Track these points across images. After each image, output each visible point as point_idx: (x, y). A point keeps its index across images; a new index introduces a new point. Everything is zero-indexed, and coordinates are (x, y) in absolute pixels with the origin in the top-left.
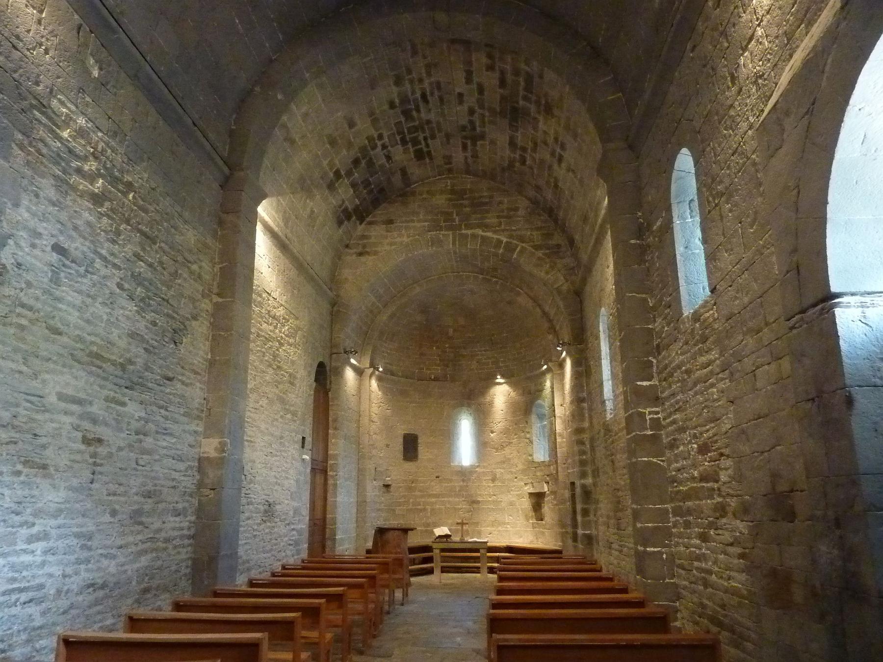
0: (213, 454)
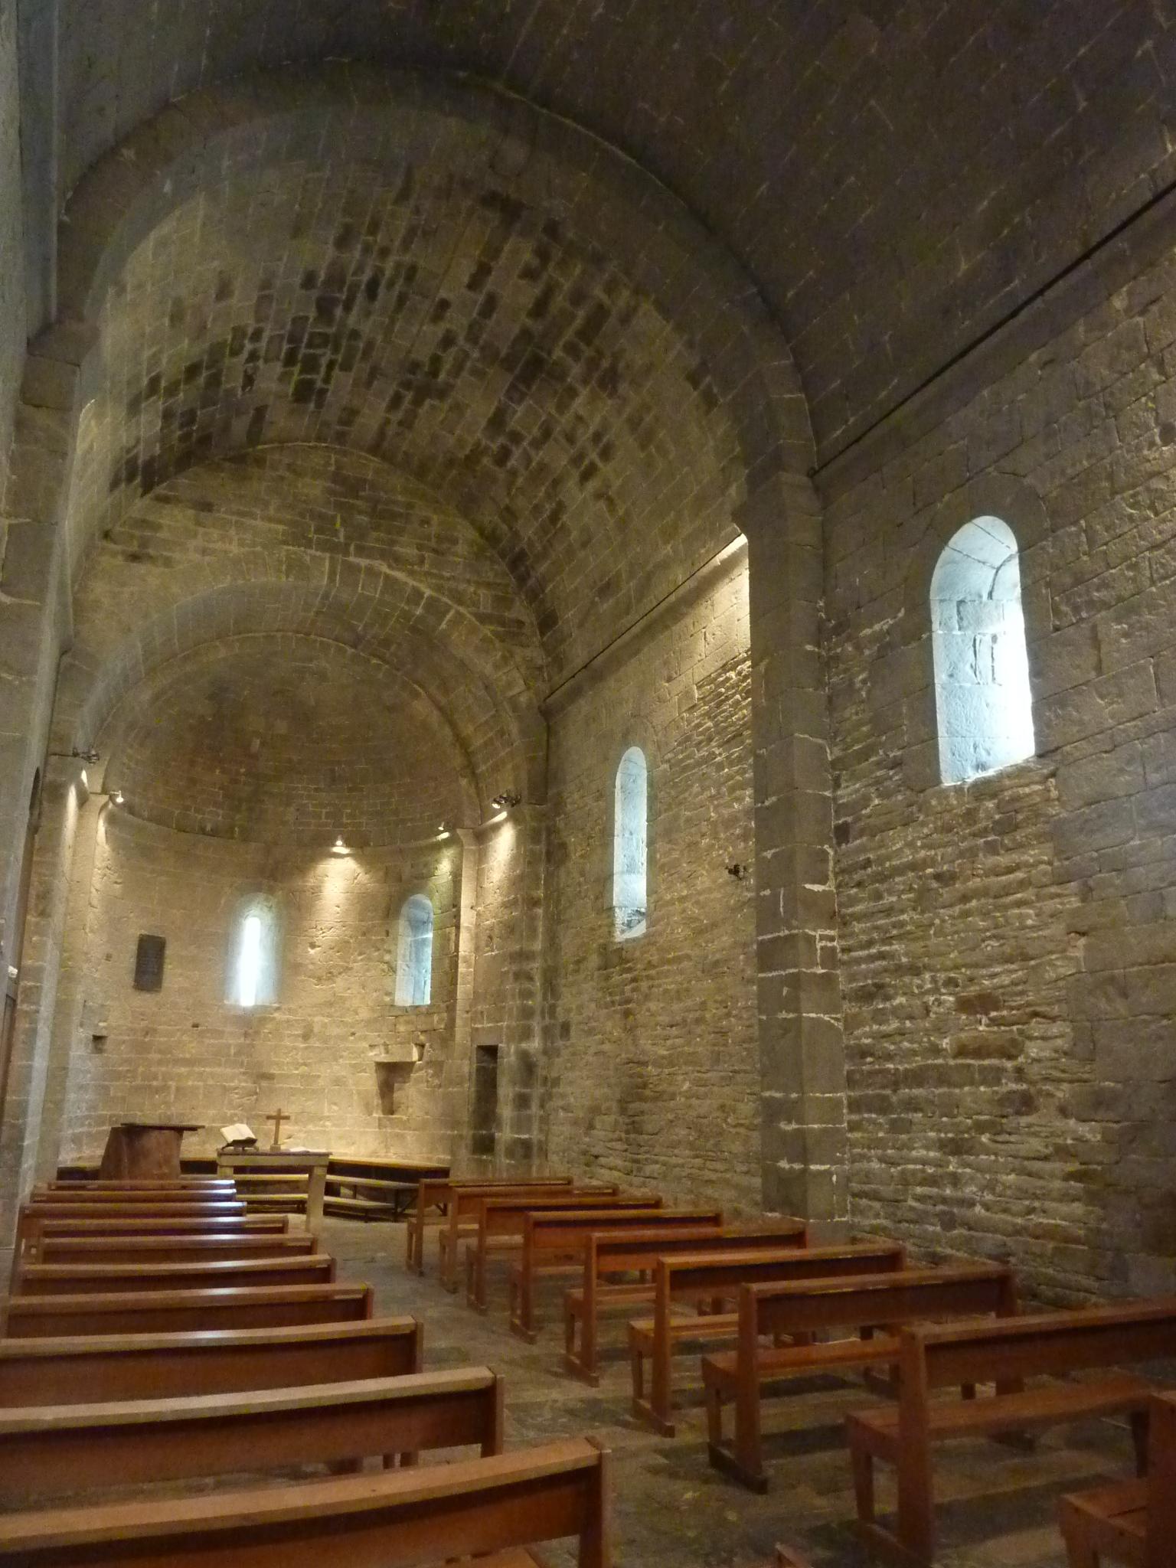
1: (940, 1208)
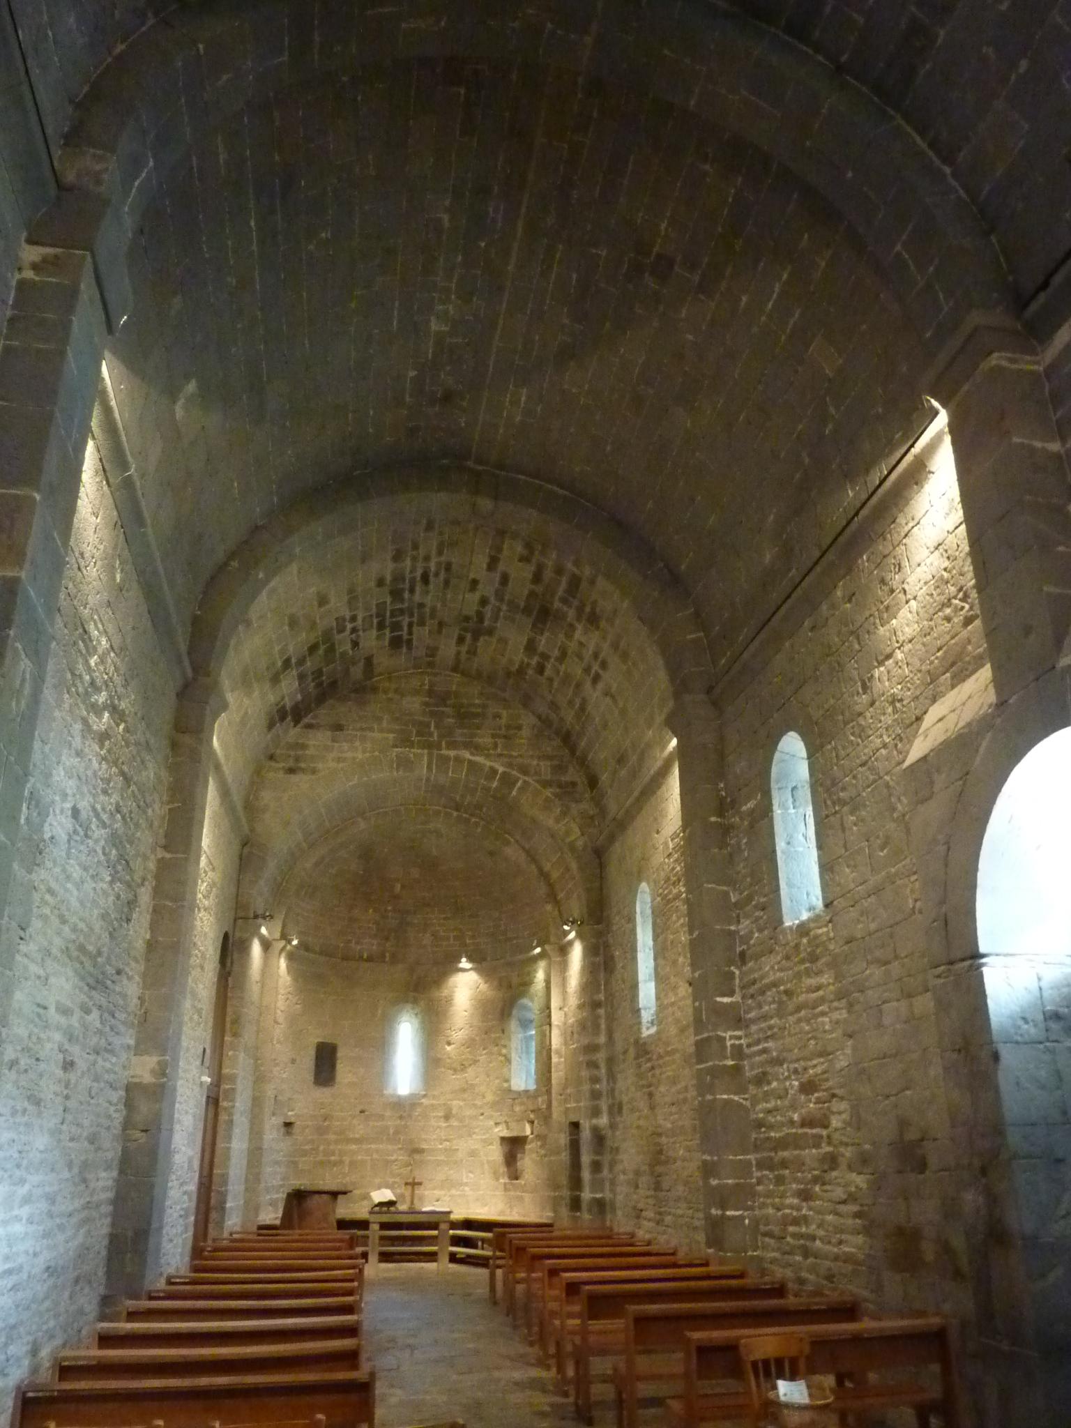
0: (148, 1078)
1: (802, 1242)
